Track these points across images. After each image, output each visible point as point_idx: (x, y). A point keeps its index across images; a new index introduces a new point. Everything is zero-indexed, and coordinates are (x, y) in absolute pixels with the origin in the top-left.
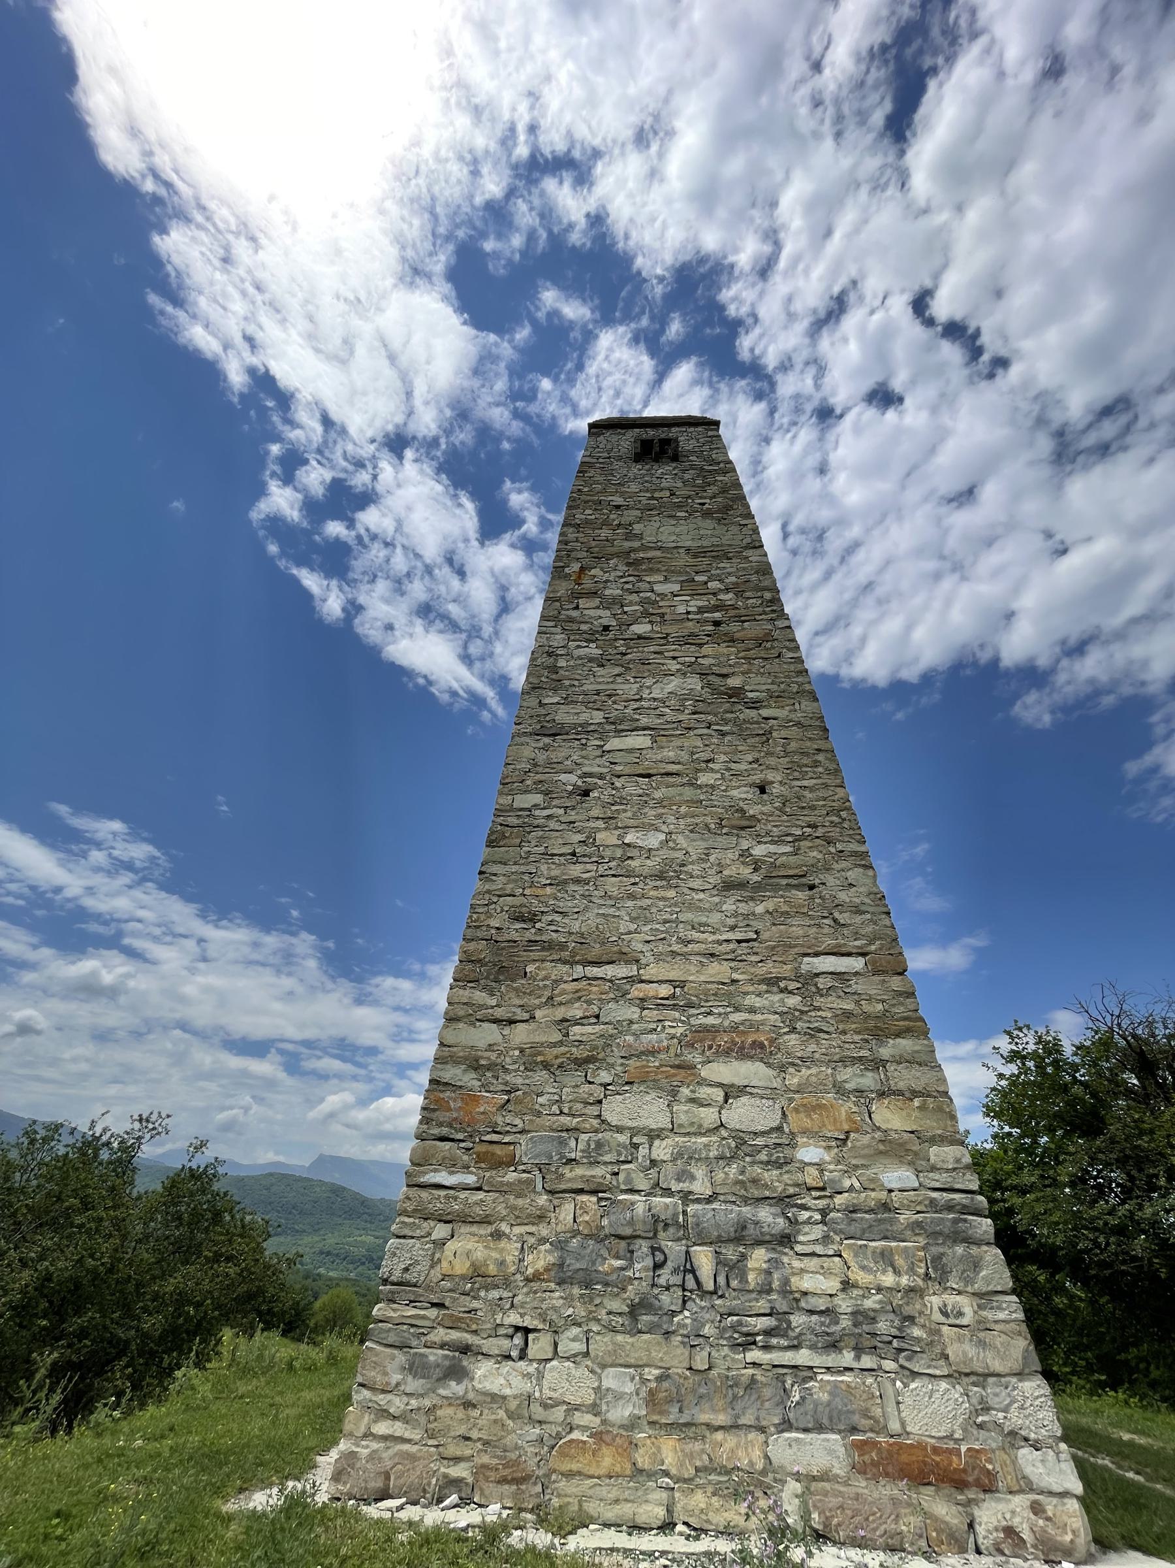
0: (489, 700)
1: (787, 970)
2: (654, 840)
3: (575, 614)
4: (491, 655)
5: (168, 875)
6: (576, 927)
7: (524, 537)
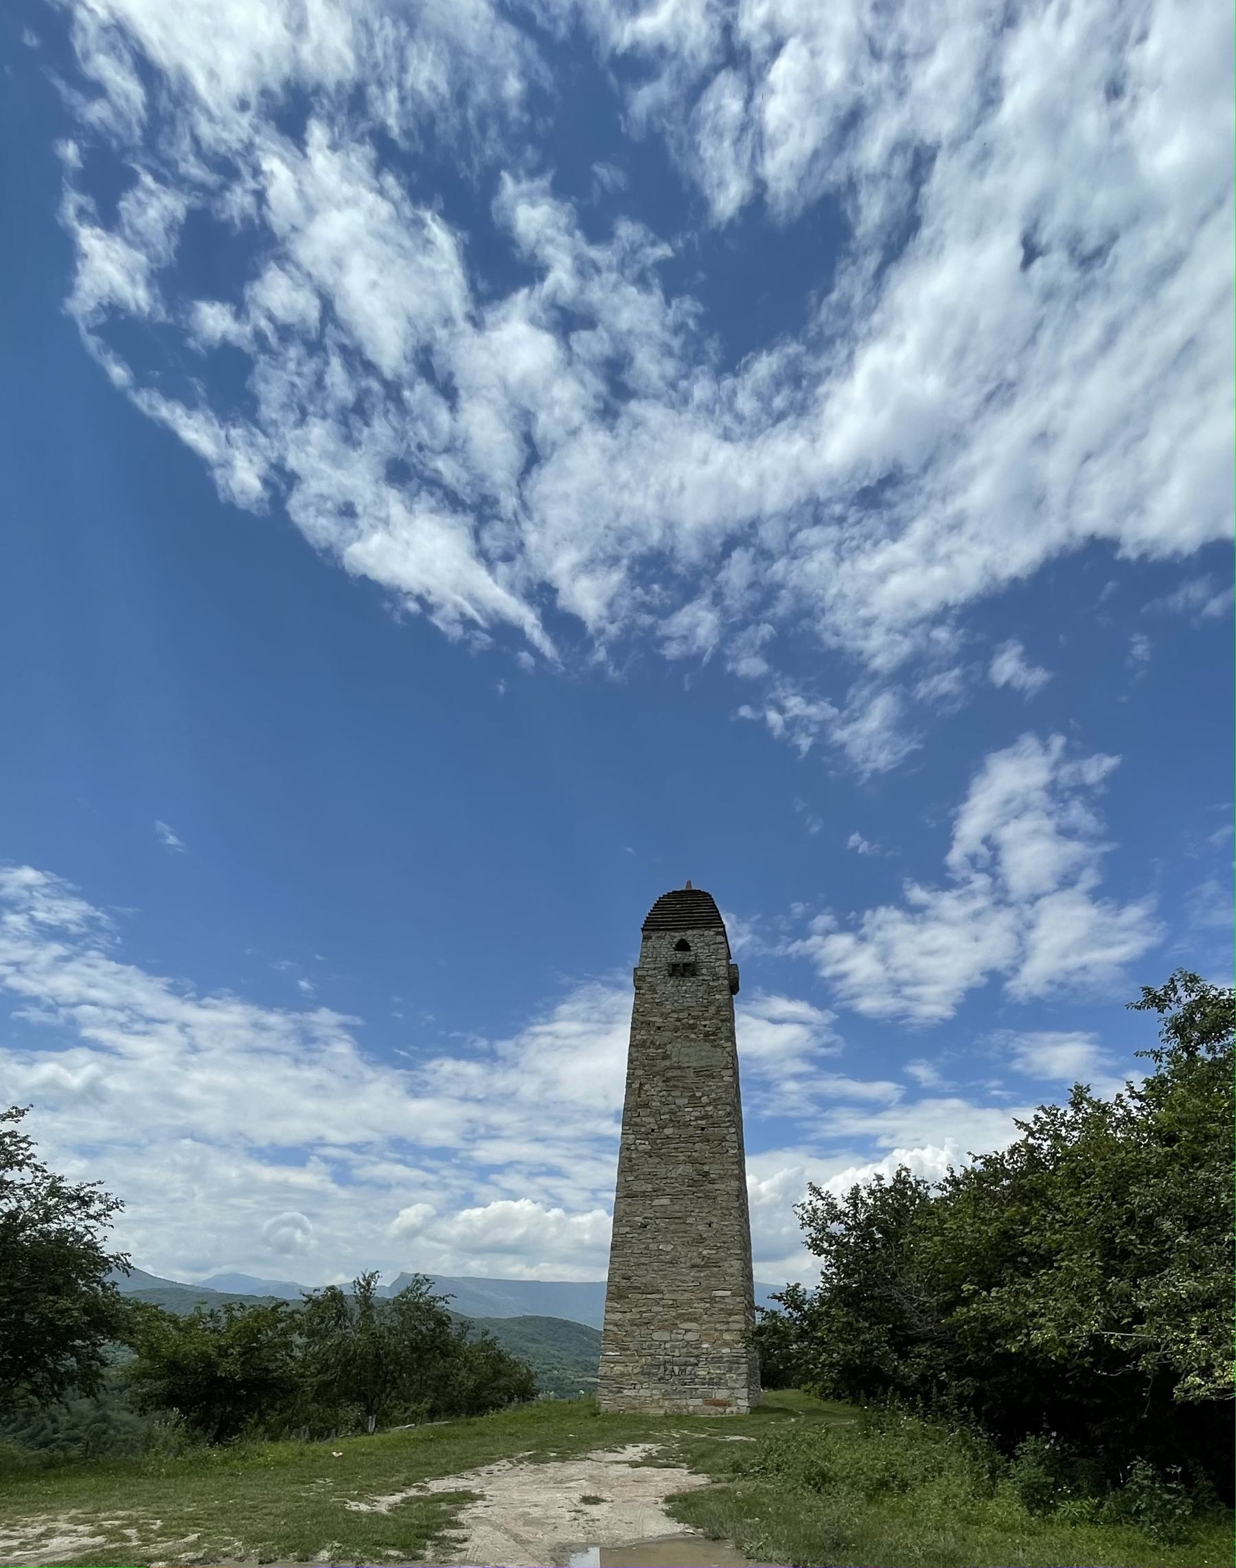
0: (528, 629)
1: (707, 1296)
2: (670, 1248)
3: (638, 1120)
4: (521, 546)
5: (119, 940)
6: (643, 1281)
7: (553, 304)
